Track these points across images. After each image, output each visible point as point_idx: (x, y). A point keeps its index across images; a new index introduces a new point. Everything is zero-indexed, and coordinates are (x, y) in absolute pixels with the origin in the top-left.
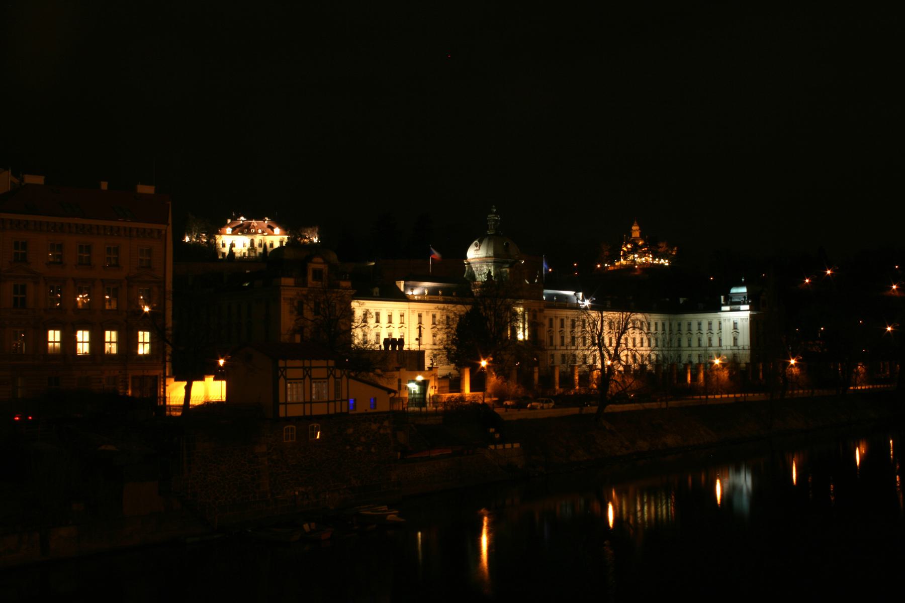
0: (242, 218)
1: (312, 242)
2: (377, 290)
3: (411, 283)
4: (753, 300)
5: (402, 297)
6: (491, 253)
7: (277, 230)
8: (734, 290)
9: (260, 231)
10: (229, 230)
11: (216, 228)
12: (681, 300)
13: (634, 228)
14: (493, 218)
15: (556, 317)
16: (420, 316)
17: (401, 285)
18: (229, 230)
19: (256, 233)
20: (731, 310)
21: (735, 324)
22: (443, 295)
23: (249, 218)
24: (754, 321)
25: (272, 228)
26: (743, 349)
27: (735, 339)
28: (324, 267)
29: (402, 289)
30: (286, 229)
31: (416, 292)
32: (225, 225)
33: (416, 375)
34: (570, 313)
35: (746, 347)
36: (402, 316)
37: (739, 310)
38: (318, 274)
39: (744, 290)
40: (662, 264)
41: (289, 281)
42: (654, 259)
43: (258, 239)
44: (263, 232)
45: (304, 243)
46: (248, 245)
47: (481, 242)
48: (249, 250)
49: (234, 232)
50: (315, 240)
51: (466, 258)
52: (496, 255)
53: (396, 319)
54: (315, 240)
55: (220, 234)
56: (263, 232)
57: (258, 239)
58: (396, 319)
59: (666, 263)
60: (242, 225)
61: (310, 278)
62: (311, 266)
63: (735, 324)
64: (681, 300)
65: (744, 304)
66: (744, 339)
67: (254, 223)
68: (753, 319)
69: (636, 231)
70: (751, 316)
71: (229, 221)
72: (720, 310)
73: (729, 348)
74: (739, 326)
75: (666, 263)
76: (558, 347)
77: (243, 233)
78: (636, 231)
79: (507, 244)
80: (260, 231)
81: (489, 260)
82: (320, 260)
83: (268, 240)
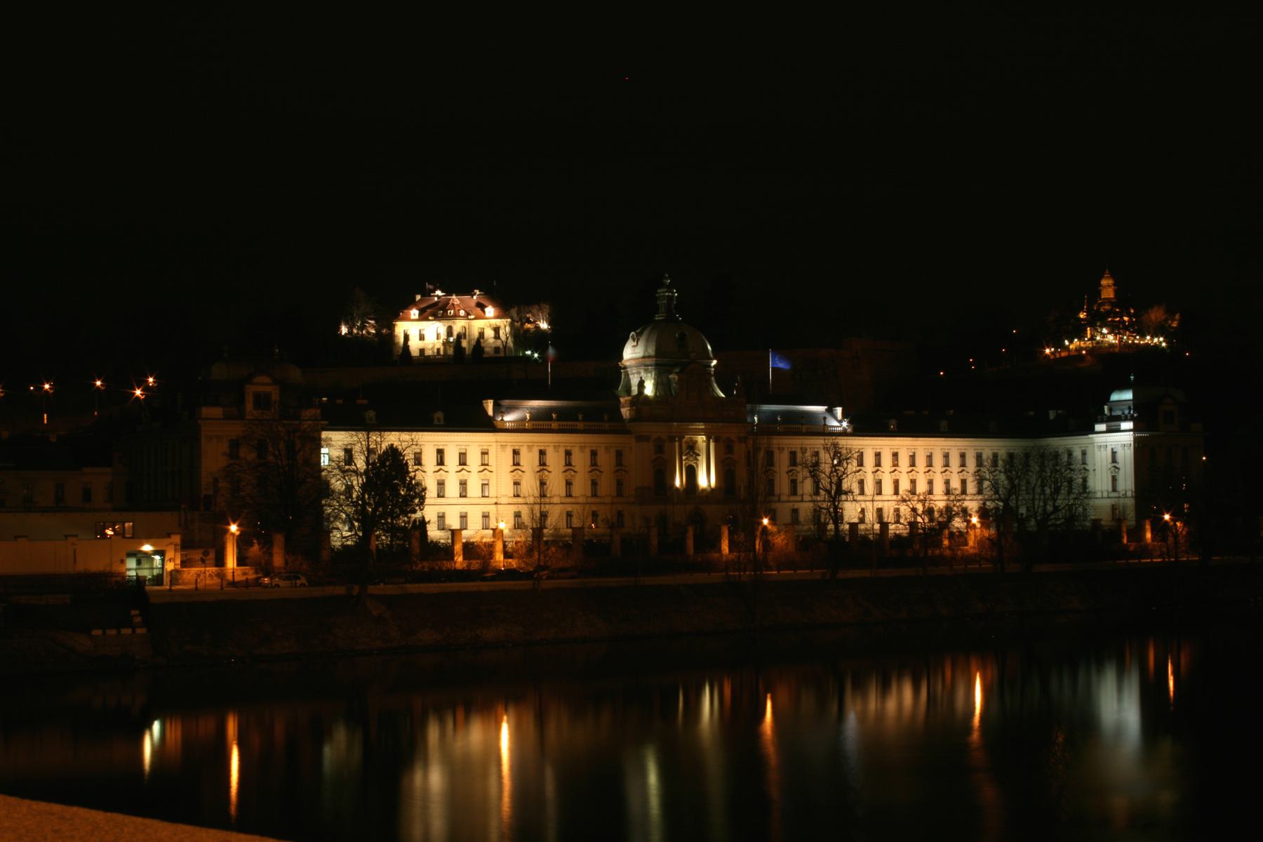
0: (439, 293)
1: (537, 328)
2: (439, 415)
3: (506, 402)
4: (1143, 416)
5: (487, 425)
6: (651, 351)
7: (490, 311)
8: (1115, 397)
9: (462, 313)
10: (414, 313)
11: (396, 311)
12: (1052, 415)
13: (1104, 282)
14: (668, 294)
15: (781, 450)
16: (542, 453)
17: (489, 406)
18: (414, 313)
19: (456, 316)
20: (1109, 431)
21: (1114, 453)
22: (558, 419)
23: (449, 292)
24: (1140, 447)
25: (481, 306)
26: (1125, 496)
27: (1114, 479)
28: (275, 392)
29: (490, 413)
30: (504, 312)
31: (510, 418)
32: (411, 303)
33: (142, 544)
34: (818, 442)
35: (1129, 494)
36: (484, 453)
37: (1119, 430)
38: (262, 401)
39: (1128, 395)
40: (1157, 347)
41: (217, 412)
42: (1152, 339)
43: (458, 326)
44: (468, 314)
45: (528, 330)
46: (443, 336)
47: (639, 335)
48: (444, 344)
49: (423, 317)
50: (544, 325)
51: (621, 358)
52: (659, 353)
53: (474, 460)
54: (544, 325)
55: (402, 319)
56: (468, 314)
57: (458, 326)
58: (474, 460)
59: (1159, 341)
60: (436, 304)
61: (249, 406)
62: (251, 390)
63: (1114, 453)
64: (1052, 415)
65: (1126, 419)
66: (1127, 482)
67: (455, 299)
68: (1139, 445)
69: (1108, 288)
70: (1135, 439)
71: (418, 297)
72: (1093, 431)
73: (1105, 495)
74: (1120, 457)
75: (1159, 341)
76: (784, 498)
77: (437, 318)
78: (1108, 288)
79: (682, 336)
80: (462, 313)
81: (648, 361)
82: (266, 379)
83: (477, 326)
